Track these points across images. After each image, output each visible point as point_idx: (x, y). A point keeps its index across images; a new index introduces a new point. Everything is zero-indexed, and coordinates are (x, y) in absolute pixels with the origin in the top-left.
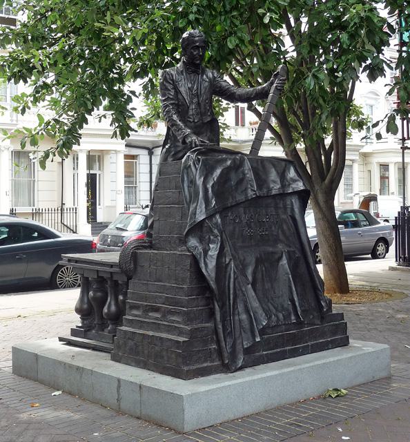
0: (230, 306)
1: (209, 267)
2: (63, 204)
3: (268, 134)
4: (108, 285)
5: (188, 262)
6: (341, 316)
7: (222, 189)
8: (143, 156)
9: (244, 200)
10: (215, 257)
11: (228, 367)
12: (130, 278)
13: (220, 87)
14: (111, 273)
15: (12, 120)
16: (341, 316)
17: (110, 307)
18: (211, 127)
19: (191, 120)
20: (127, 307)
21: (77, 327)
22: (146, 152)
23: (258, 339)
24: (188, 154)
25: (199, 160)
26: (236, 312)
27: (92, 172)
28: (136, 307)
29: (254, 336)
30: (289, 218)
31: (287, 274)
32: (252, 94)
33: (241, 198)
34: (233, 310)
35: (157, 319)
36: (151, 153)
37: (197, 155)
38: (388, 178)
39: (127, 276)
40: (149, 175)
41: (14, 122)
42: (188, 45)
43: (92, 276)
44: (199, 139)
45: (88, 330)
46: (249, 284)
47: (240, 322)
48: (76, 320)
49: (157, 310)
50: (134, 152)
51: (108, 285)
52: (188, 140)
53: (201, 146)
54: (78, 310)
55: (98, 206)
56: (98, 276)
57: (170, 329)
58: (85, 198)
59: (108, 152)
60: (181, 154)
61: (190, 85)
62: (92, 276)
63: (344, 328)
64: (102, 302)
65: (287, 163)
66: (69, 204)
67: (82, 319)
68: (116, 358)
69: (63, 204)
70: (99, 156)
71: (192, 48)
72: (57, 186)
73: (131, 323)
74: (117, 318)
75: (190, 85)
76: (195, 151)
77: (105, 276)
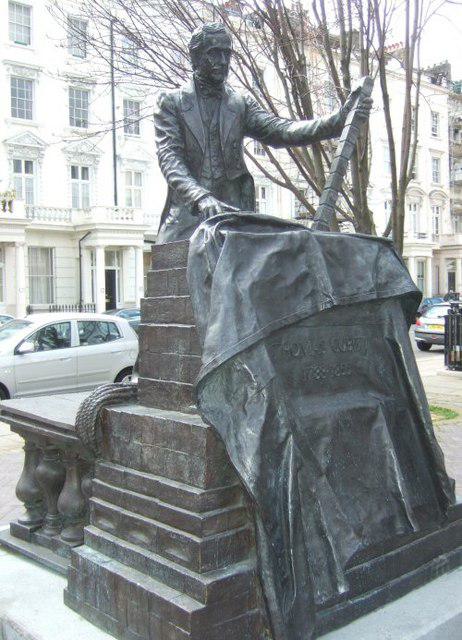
0: (288, 525)
2: (81, 300)
7: (268, 292)
9: (310, 312)
13: (257, 121)
15: (28, 217)
17: (68, 497)
18: (237, 186)
21: (19, 522)
25: (222, 237)
26: (300, 538)
27: (110, 268)
29: (335, 586)
30: (387, 342)
32: (311, 130)
33: (304, 307)
34: (295, 532)
37: (218, 228)
42: (202, 47)
44: (223, 204)
45: (35, 530)
46: (321, 475)
48: (20, 513)
52: (203, 205)
54: (20, 494)
58: (104, 295)
59: (126, 248)
64: (57, 486)
66: (87, 300)
67: (29, 510)
69: (81, 300)
71: (208, 53)
73: (98, 543)
75: (206, 118)
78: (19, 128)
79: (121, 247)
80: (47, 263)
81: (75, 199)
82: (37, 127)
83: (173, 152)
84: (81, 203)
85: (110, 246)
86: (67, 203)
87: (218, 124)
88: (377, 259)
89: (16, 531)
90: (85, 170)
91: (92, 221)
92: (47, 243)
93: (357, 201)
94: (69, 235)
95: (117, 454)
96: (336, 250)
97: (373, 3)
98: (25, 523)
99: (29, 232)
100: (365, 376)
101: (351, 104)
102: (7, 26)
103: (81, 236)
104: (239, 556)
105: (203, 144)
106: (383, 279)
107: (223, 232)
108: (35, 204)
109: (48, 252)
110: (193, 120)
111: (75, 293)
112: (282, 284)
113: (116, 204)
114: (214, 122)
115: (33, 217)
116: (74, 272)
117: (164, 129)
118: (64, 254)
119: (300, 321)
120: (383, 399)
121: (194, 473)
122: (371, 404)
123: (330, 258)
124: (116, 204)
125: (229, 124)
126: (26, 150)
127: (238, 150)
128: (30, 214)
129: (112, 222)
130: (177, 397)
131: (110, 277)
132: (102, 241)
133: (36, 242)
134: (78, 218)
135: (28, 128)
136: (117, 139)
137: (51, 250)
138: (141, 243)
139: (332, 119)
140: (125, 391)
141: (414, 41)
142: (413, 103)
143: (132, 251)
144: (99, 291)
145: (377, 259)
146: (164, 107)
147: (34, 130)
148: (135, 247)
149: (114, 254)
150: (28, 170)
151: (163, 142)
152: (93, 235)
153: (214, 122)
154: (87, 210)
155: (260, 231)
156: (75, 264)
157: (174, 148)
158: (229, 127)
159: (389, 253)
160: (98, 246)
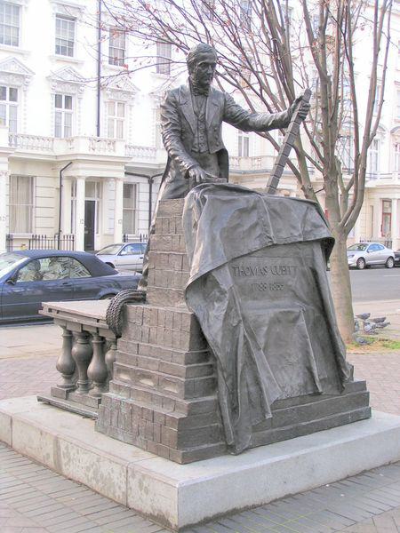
1: (214, 332)
2: (60, 231)
3: (287, 169)
4: (94, 341)
5: (188, 322)
6: (363, 385)
8: (143, 187)
10: (222, 318)
11: (230, 449)
12: (118, 336)
14: (97, 328)
15: (10, 145)
16: (363, 385)
19: (197, 150)
20: (115, 370)
22: (146, 180)
23: (269, 416)
24: (192, 192)
28: (126, 371)
29: (264, 412)
31: (305, 337)
35: (150, 387)
36: (151, 182)
38: (390, 214)
39: (116, 333)
40: (148, 204)
41: (13, 147)
42: (196, 61)
43: (76, 330)
45: (70, 391)
47: (249, 396)
49: (149, 377)
50: (133, 180)
51: (94, 341)
52: (192, 173)
53: (208, 181)
55: (96, 235)
56: (188, 170)
57: (164, 401)
59: (107, 179)
60: (182, 191)
61: (196, 109)
62: (76, 330)
63: (364, 399)
65: (309, 205)
66: (66, 231)
68: (103, 430)
69: (60, 231)
70: (98, 184)
72: (54, 212)
73: (118, 388)
74: (103, 380)
75: (196, 109)
76: (200, 188)
77: (90, 331)
78: (7, 55)
79: (101, 178)
80: (28, 190)
81: (57, 127)
82: (22, 54)
83: (173, 134)
84: (62, 130)
85: (91, 177)
86: (48, 131)
87: (205, 114)
88: (305, 215)
89: (54, 392)
90: (68, 99)
91: (75, 151)
92: (29, 172)
93: (327, 153)
94: (51, 164)
95: (133, 334)
96: (278, 208)
97: (333, 7)
98: (62, 387)
99: (12, 160)
100: (293, 291)
101: (295, 107)
102: (53, 21)
103: (61, 167)
104: (208, 393)
105: (193, 128)
106: (308, 228)
107: (206, 196)
108: (18, 132)
109: (30, 180)
110: (189, 110)
111: (53, 223)
112: (240, 230)
113: (98, 135)
114: (202, 112)
115: (16, 145)
116: (54, 203)
117: (168, 116)
118: (44, 188)
119: (253, 253)
120: (305, 307)
121: (182, 343)
122: (297, 310)
123: (273, 213)
124: (98, 135)
125: (212, 113)
126: (11, 77)
127: (217, 130)
128: (13, 142)
129: (88, 153)
130: (173, 298)
131: (90, 209)
132: (83, 172)
133: (18, 172)
134: (60, 149)
135: (13, 56)
136: (102, 69)
137: (32, 178)
138: (122, 175)
139: (283, 116)
140: (138, 295)
141: (384, 12)
142: (380, 74)
143: (112, 183)
144: (78, 221)
145: (305, 215)
146: (168, 102)
147: (19, 58)
148: (116, 179)
149: (94, 185)
150: (68, 105)
151: (166, 126)
152: (74, 166)
153: (202, 112)
154: (70, 141)
155: (228, 195)
156: (55, 193)
157: (174, 131)
158: (212, 116)
159: (315, 211)
160: (79, 177)
